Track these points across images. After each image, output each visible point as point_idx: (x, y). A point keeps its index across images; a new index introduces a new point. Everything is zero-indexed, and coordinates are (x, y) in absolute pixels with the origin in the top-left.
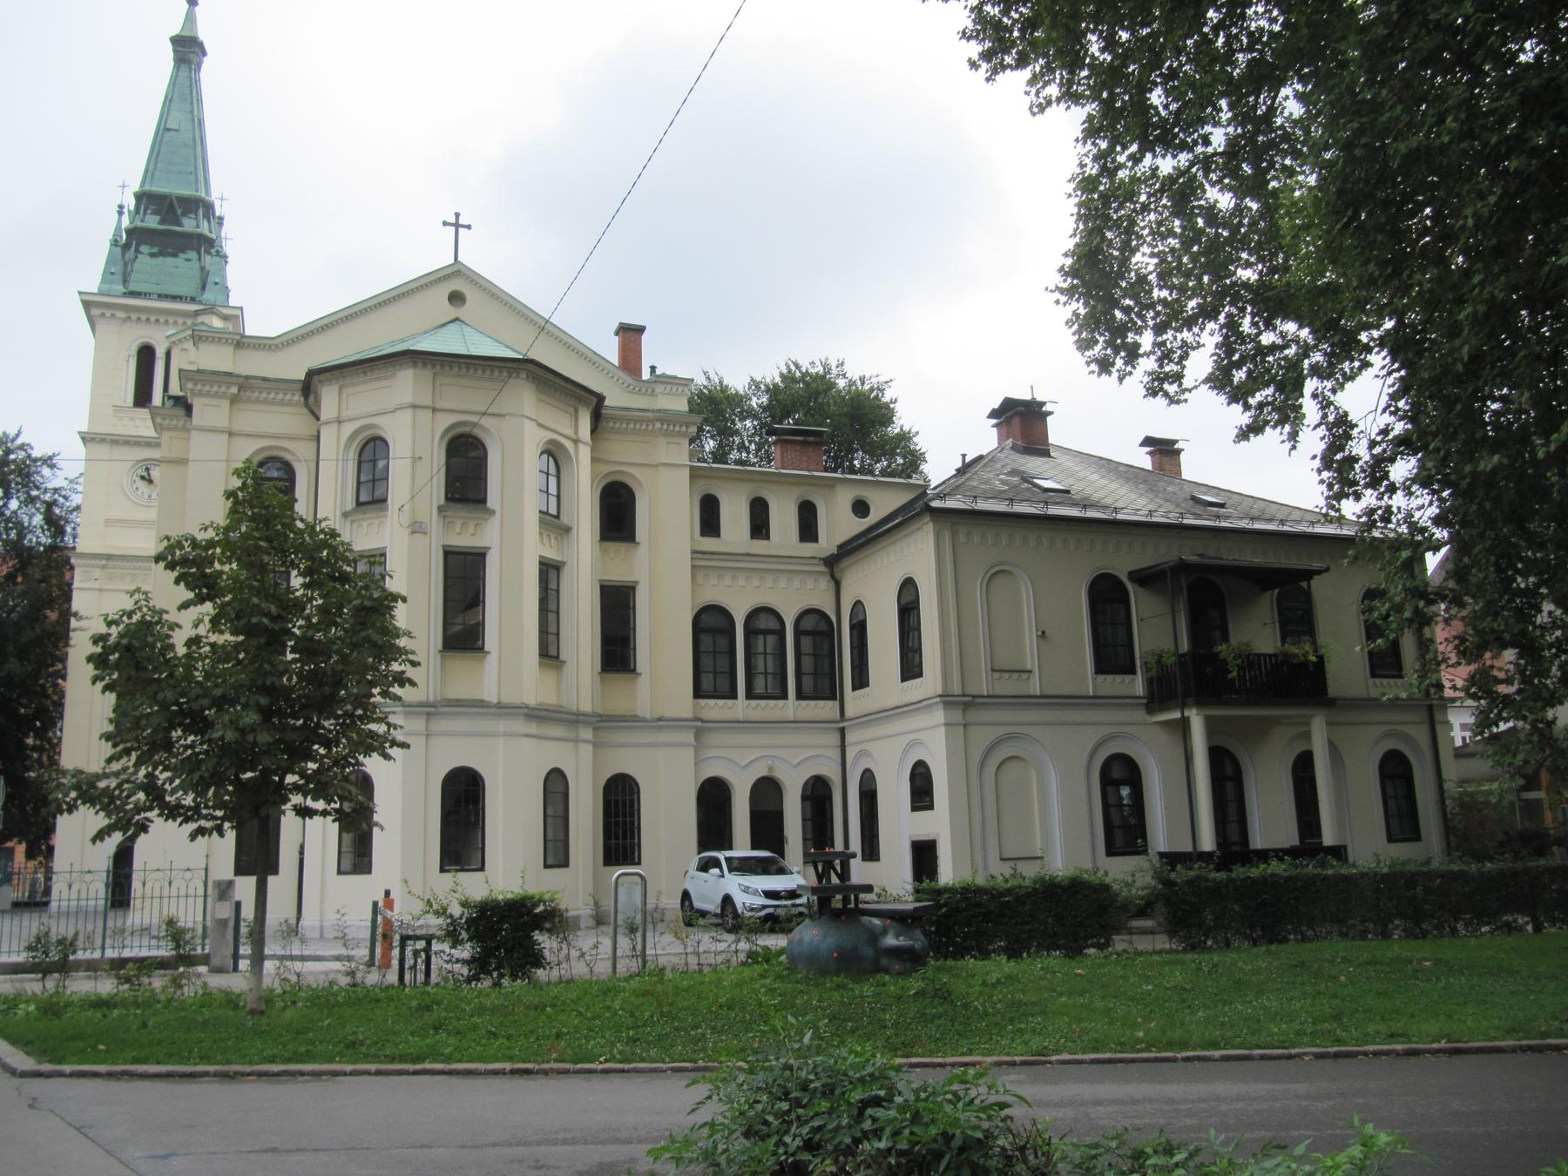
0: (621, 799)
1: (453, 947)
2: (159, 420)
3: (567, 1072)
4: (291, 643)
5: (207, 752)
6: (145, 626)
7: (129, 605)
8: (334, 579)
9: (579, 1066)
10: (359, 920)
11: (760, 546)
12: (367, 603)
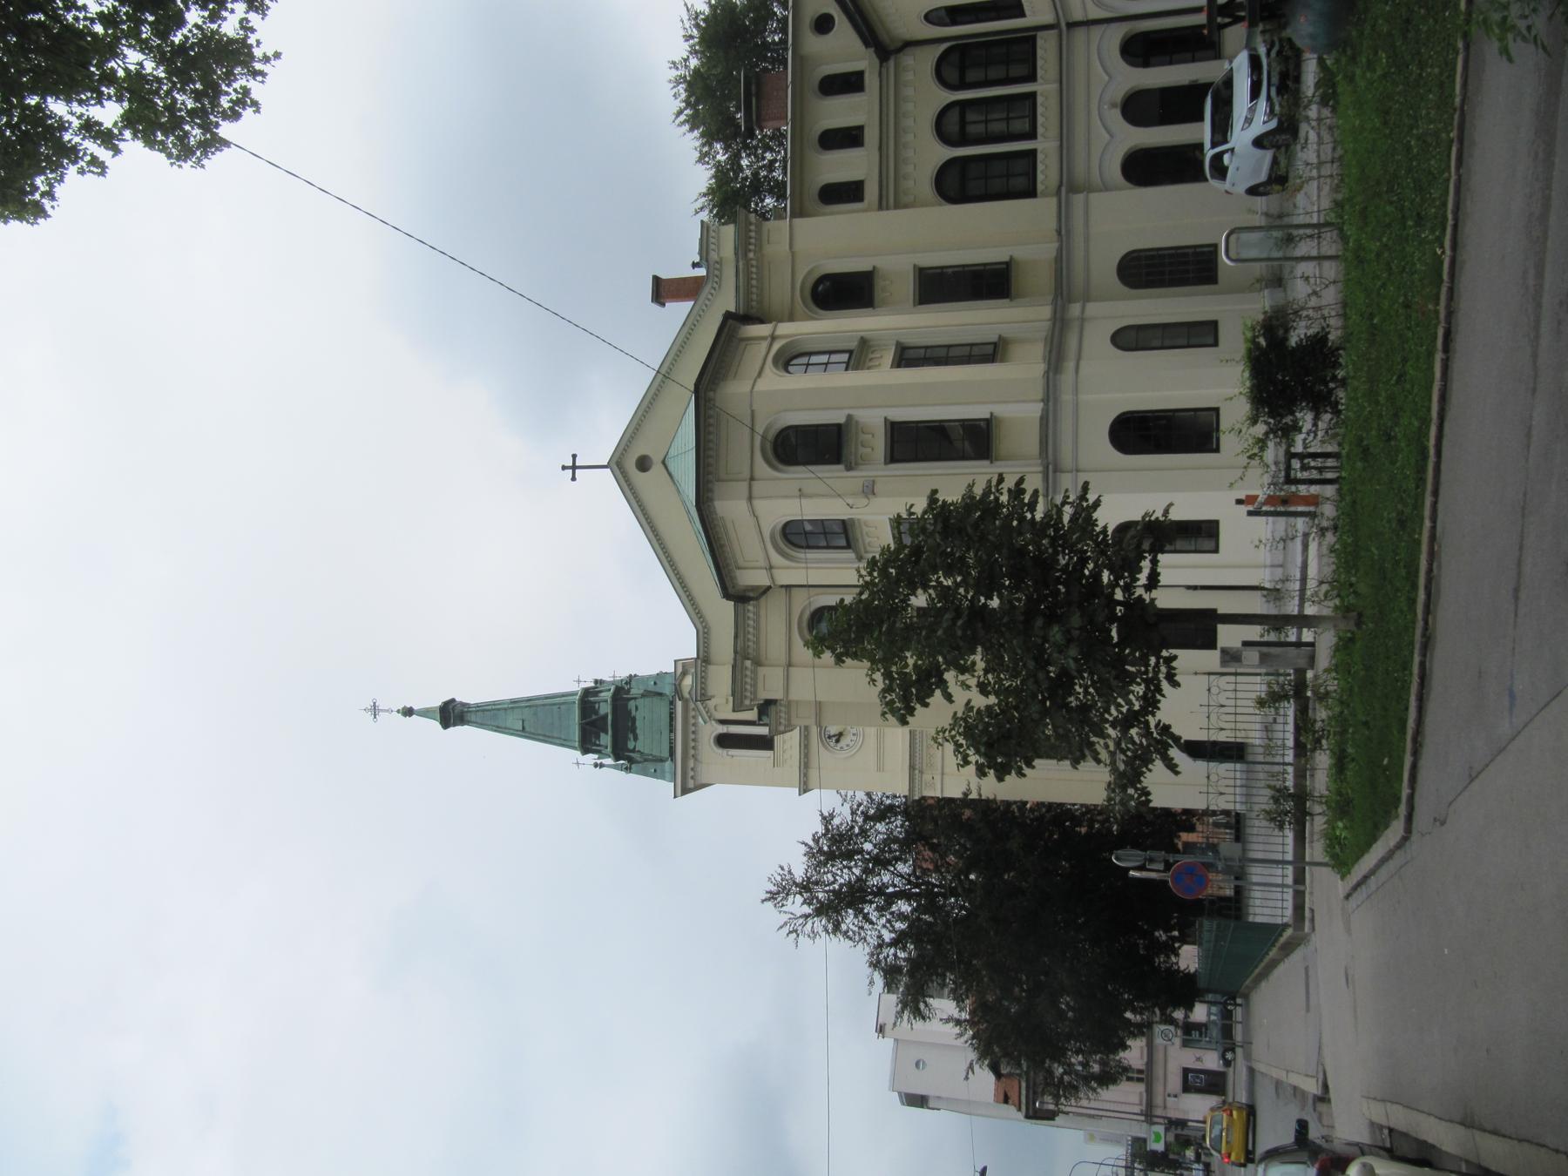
0: (1145, 269)
1: (1299, 430)
2: (782, 728)
3: (1451, 290)
4: (983, 599)
5: (1091, 674)
6: (969, 732)
7: (950, 747)
8: (917, 562)
9: (1445, 277)
10: (1264, 527)
11: (871, 136)
12: (939, 526)
